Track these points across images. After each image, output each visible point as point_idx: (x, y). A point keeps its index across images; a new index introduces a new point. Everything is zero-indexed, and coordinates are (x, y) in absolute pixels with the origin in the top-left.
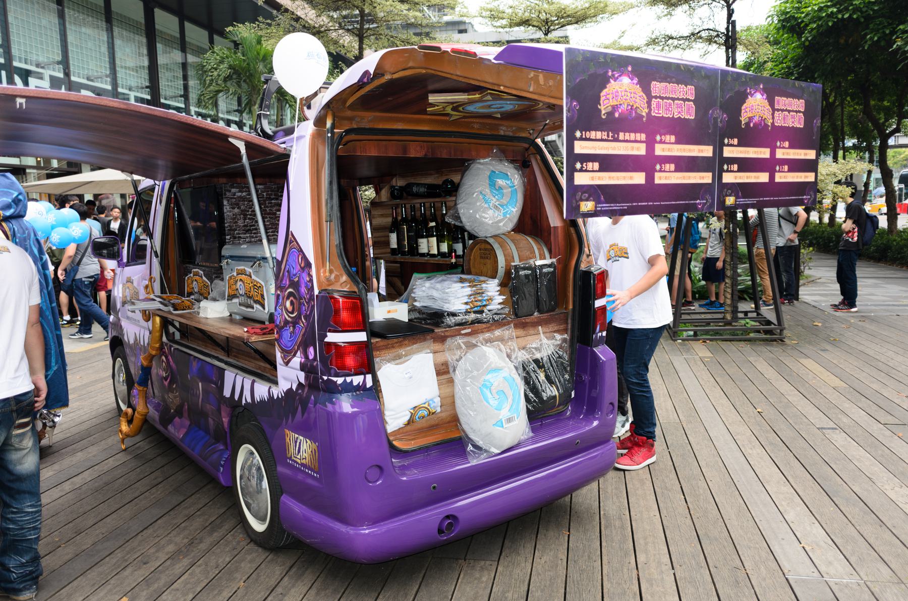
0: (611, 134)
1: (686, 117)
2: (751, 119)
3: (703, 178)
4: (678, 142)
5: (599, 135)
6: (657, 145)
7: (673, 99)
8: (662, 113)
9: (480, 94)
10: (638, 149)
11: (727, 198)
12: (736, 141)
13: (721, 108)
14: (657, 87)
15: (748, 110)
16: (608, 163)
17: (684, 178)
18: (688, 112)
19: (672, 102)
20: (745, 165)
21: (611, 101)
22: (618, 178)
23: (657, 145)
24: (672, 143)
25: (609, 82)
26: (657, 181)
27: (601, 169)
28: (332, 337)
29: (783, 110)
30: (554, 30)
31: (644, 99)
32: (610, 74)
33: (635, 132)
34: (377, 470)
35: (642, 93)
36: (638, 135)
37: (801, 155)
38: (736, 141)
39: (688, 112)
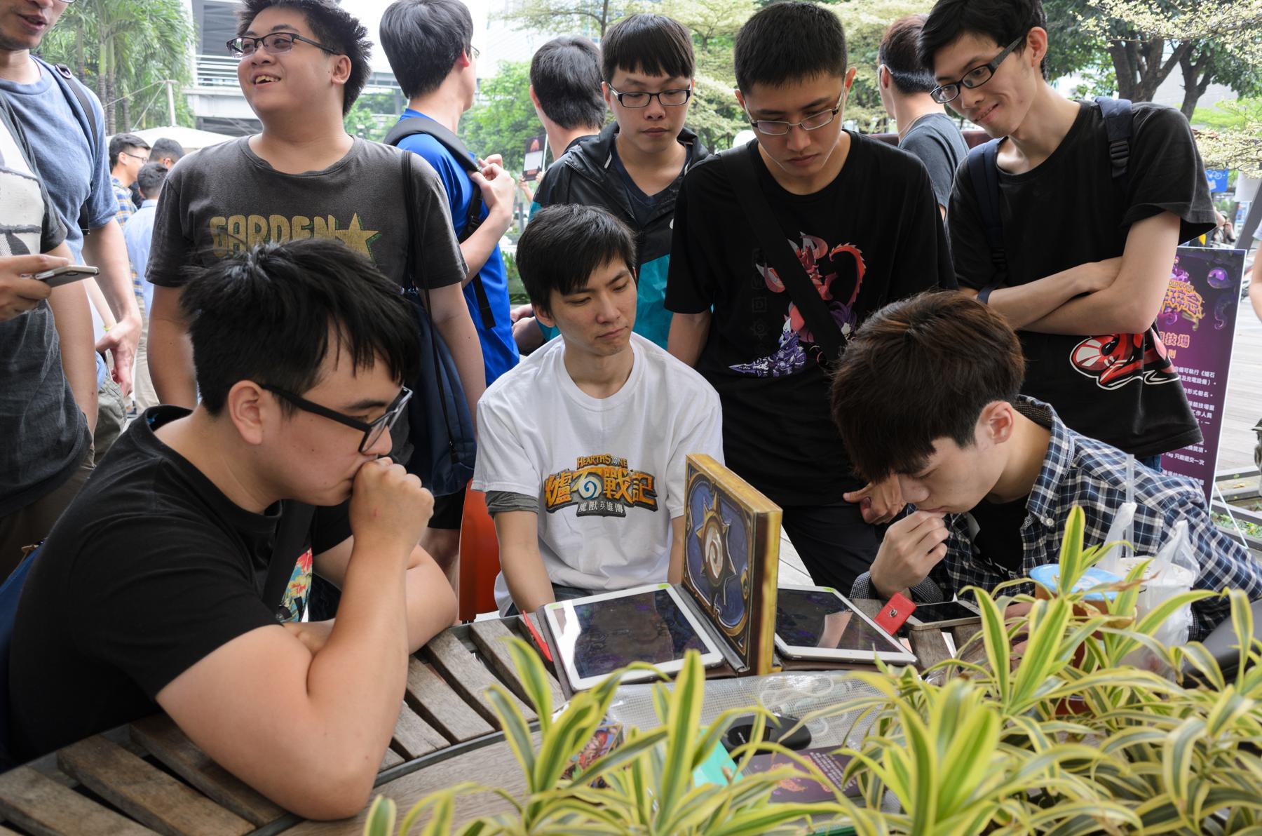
9: (773, 132)
30: (811, 757)
31: (1197, 300)
33: (1184, 367)
35: (1194, 293)
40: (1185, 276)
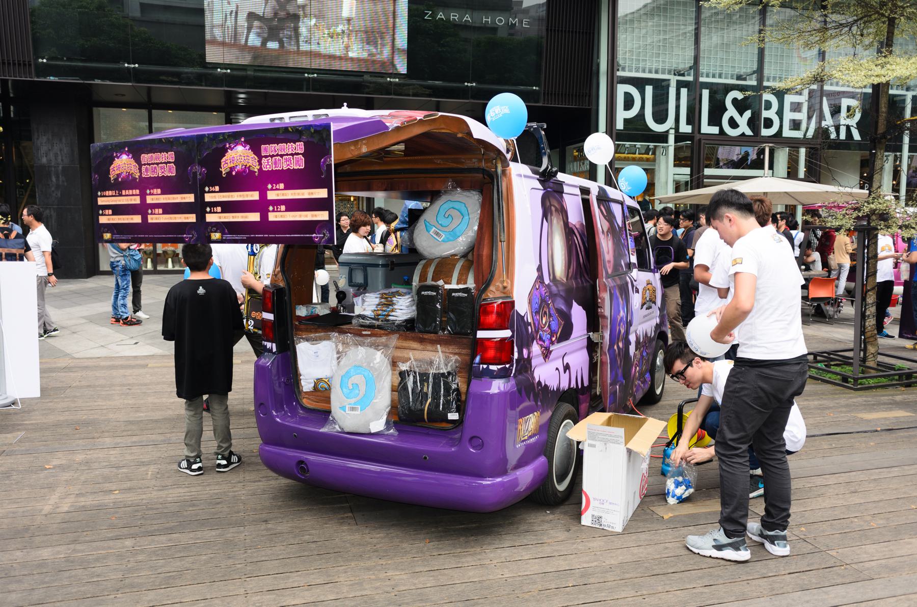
0: (117, 192)
1: (169, 175)
2: (119, 175)
3: (188, 218)
4: (163, 193)
5: (110, 193)
6: (147, 197)
7: (157, 164)
8: (150, 175)
10: (135, 200)
11: (105, 235)
12: (217, 188)
13: (199, 164)
14: (145, 158)
15: (115, 169)
16: (118, 210)
17: (171, 218)
18: (170, 171)
19: (280, 158)
20: (293, 205)
21: (229, 164)
22: (124, 219)
23: (147, 197)
24: (159, 194)
25: (114, 160)
26: (150, 221)
27: (113, 214)
28: (481, 334)
29: (272, 156)
32: (228, 146)
33: (132, 189)
34: (262, 406)
35: (253, 155)
36: (134, 191)
37: (292, 194)
38: (217, 188)
39: (170, 171)
40: (248, 147)
